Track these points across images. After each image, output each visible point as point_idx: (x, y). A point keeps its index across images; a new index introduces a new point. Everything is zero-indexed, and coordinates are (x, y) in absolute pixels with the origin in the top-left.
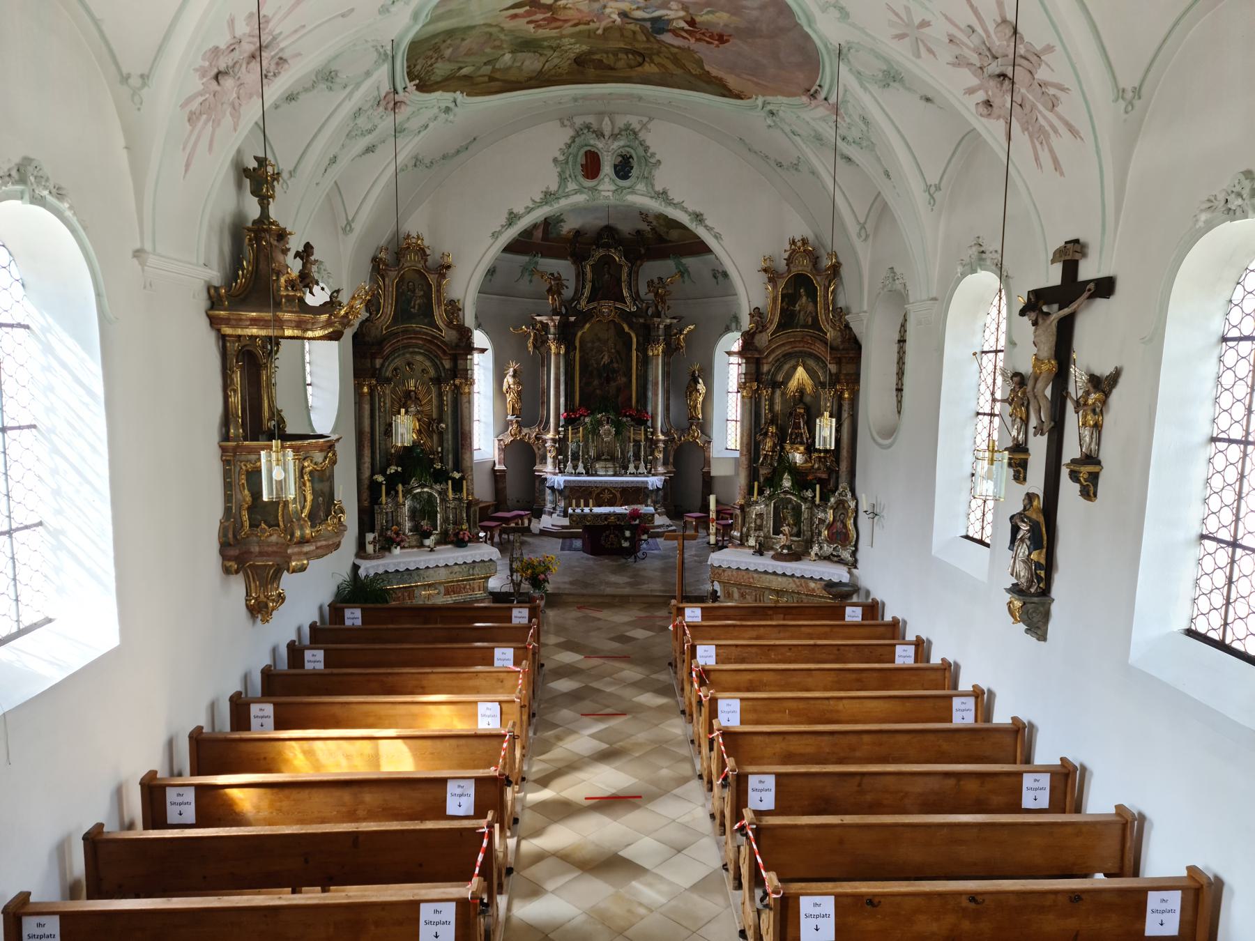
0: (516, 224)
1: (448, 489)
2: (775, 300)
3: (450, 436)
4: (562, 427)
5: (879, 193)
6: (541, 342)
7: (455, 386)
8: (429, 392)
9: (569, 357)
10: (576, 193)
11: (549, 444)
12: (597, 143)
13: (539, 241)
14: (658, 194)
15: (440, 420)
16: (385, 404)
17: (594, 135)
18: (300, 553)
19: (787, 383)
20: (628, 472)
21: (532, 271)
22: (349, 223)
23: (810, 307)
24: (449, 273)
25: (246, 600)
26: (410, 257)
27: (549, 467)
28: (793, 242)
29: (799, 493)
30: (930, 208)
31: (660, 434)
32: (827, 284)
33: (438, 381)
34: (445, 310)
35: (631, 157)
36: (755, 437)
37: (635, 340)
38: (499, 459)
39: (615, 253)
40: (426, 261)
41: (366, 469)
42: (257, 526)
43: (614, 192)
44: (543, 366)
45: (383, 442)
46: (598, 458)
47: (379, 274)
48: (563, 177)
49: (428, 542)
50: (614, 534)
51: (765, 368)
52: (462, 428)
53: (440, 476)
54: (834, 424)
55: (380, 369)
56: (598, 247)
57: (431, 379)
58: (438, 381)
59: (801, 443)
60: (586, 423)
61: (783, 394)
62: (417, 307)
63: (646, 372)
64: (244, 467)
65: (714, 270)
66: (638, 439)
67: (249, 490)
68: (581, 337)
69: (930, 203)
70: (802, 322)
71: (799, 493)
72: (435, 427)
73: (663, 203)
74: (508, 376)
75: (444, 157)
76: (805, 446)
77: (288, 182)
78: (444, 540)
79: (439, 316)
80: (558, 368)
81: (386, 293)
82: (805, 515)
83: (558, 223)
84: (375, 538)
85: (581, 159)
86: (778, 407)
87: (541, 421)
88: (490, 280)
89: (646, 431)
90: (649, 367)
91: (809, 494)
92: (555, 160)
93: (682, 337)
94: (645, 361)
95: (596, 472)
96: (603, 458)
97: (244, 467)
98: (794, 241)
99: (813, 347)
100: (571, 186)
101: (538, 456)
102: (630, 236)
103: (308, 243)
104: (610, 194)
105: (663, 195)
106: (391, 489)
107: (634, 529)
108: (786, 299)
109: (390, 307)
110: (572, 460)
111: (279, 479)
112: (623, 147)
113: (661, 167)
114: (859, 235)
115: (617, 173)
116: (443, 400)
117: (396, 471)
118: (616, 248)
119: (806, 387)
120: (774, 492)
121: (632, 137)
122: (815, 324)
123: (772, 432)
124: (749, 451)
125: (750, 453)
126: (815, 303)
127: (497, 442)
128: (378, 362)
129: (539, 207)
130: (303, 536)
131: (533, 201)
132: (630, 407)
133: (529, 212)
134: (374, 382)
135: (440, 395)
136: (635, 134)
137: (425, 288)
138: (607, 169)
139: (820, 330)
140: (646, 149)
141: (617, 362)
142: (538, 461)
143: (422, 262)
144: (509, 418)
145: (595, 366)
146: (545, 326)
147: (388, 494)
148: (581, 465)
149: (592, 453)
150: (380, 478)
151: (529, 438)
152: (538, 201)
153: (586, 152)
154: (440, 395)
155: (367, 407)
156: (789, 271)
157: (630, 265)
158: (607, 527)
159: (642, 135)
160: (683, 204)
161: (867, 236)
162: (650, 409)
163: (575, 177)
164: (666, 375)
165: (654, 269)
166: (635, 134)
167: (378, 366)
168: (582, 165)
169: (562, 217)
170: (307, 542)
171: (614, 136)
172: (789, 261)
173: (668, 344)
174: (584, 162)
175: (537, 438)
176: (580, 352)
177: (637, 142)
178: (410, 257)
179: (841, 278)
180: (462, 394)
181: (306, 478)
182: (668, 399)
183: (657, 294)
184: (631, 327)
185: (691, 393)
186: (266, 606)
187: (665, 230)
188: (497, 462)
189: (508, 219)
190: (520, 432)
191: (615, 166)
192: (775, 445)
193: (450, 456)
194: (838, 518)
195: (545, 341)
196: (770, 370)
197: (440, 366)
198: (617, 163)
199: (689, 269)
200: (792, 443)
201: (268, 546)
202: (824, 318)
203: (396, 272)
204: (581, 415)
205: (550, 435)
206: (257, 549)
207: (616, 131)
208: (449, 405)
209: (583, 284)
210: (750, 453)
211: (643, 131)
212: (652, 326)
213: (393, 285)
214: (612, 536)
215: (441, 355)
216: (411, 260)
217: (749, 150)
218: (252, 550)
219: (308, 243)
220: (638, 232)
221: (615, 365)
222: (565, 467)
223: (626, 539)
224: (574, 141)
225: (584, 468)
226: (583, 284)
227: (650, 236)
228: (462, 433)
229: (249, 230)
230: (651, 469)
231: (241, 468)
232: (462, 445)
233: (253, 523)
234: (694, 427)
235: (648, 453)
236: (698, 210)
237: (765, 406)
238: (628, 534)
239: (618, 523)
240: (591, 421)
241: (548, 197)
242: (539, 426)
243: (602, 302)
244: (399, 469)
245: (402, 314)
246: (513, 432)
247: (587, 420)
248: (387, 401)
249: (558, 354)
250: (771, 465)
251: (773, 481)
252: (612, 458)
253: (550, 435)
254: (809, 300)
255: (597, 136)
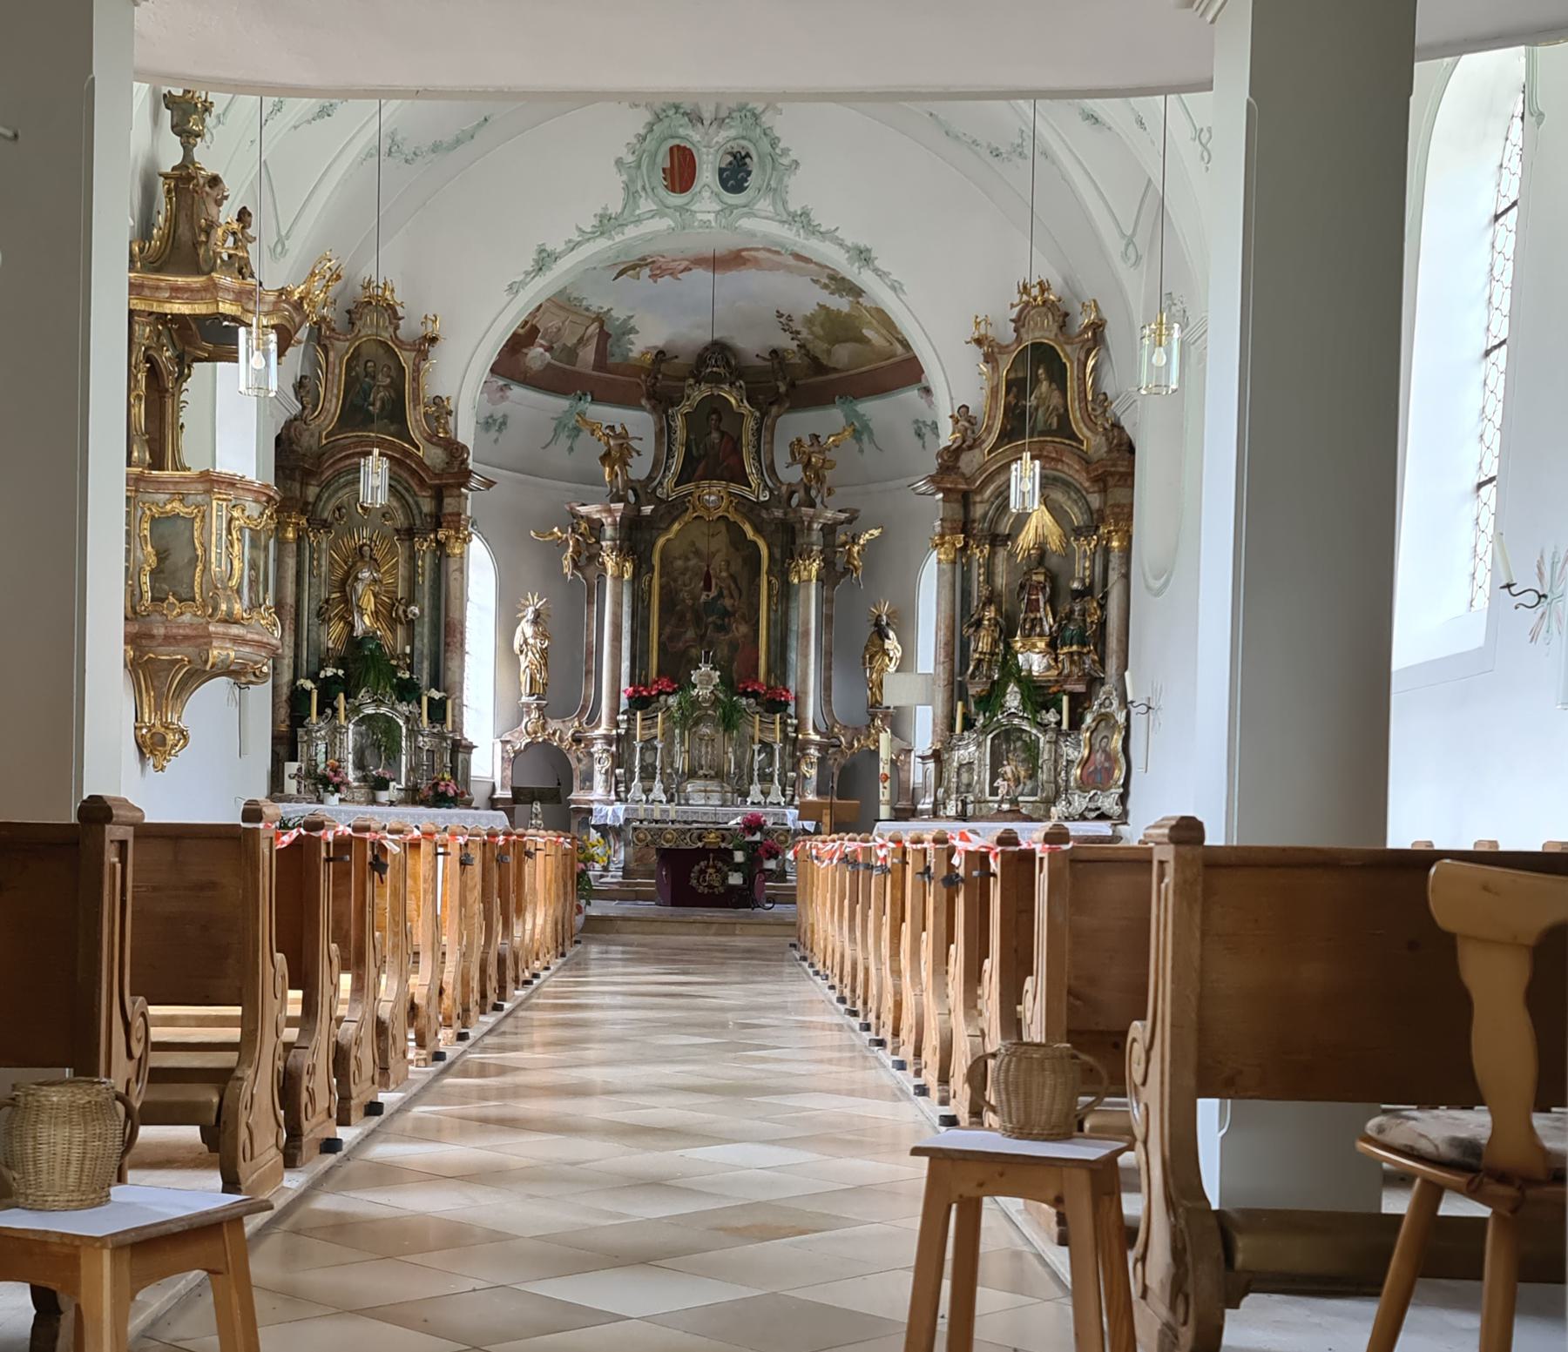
0: (550, 269)
1: (420, 714)
2: (994, 392)
3: (426, 631)
4: (623, 713)
5: (1150, 180)
6: (587, 558)
7: (438, 542)
8: (392, 552)
9: (640, 583)
10: (652, 217)
11: (598, 747)
12: (691, 133)
13: (589, 371)
14: (794, 216)
15: (411, 601)
16: (319, 565)
17: (686, 119)
18: (225, 636)
19: (1017, 536)
20: (749, 800)
21: (575, 428)
22: (281, 241)
23: (1056, 399)
24: (434, 351)
25: (136, 728)
26: (371, 320)
27: (599, 790)
28: (1025, 289)
29: (1034, 717)
30: (1203, 166)
31: (811, 731)
32: (1083, 358)
33: (408, 534)
34: (426, 414)
35: (748, 155)
36: (962, 631)
37: (764, 552)
38: (503, 778)
39: (730, 393)
40: (397, 328)
41: (286, 668)
42: (163, 600)
43: (717, 213)
44: (590, 603)
45: (313, 635)
46: (692, 774)
47: (319, 344)
48: (632, 189)
49: (383, 796)
50: (714, 867)
51: (978, 511)
52: (447, 615)
53: (407, 691)
54: (1037, 470)
55: (315, 504)
56: (698, 382)
57: (397, 531)
58: (408, 534)
59: (1041, 635)
60: (668, 708)
61: (1012, 555)
62: (378, 404)
63: (786, 614)
64: (148, 512)
65: (916, 422)
66: (769, 740)
67: (152, 547)
68: (664, 546)
69: (1203, 158)
70: (1040, 426)
71: (1034, 717)
72: (401, 612)
73: (801, 231)
74: (523, 623)
75: (435, 148)
76: (1047, 639)
77: (214, 131)
78: (413, 796)
79: (415, 419)
80: (618, 604)
81: (329, 376)
82: (1045, 754)
83: (624, 334)
84: (300, 769)
85: (663, 160)
86: (1001, 581)
87: (584, 708)
88: (496, 441)
89: (784, 723)
90: (793, 605)
91: (1051, 717)
92: (619, 162)
93: (856, 549)
94: (785, 594)
95: (687, 800)
96: (701, 773)
97: (148, 512)
98: (1025, 287)
99: (1059, 467)
100: (646, 205)
101: (576, 774)
102: (759, 362)
103: (244, 208)
104: (711, 217)
105: (803, 220)
106: (326, 703)
107: (753, 851)
108: (1014, 389)
109: (334, 400)
110: (642, 779)
111: (258, 367)
112: (735, 139)
113: (798, 172)
114: (1125, 255)
115: (724, 183)
116: (415, 566)
117: (336, 674)
118: (732, 384)
119: (1050, 539)
120: (991, 719)
121: (750, 121)
122: (1064, 428)
123: (989, 620)
124: (950, 656)
125: (952, 660)
126: (1063, 391)
127: (499, 746)
128: (312, 492)
129: (589, 240)
130: (230, 613)
131: (580, 230)
132: (756, 680)
133: (573, 249)
134: (303, 522)
135: (412, 557)
136: (756, 117)
137: (393, 373)
138: (707, 175)
139: (1073, 437)
140: (774, 143)
141: (732, 596)
142: (576, 783)
143: (391, 330)
144: (524, 699)
145: (689, 602)
146: (596, 527)
147: (320, 713)
148: (658, 786)
149: (679, 764)
150: (309, 685)
151: (561, 740)
152: (589, 230)
153: (671, 149)
154: (412, 557)
155: (291, 563)
156: (1019, 340)
157: (758, 414)
158: (703, 853)
159: (766, 120)
160: (837, 234)
161: (1138, 258)
162: (792, 684)
163: (653, 190)
164: (826, 621)
165: (797, 425)
166: (756, 117)
167: (311, 499)
168: (664, 170)
169: (632, 323)
170: (235, 623)
171: (720, 121)
172: (1019, 322)
173: (828, 563)
174: (668, 165)
175: (577, 740)
176: (661, 576)
177: (758, 130)
178: (371, 320)
179: (1108, 350)
180: (448, 556)
181: (235, 536)
182: (829, 667)
183: (807, 465)
184: (758, 530)
185: (872, 657)
186: (163, 742)
187: (825, 346)
188: (498, 785)
189: (537, 262)
190: (544, 729)
191: (721, 171)
192: (995, 643)
193: (426, 664)
194: (1097, 746)
195: (594, 557)
196: (986, 514)
197: (414, 507)
198: (723, 166)
199: (871, 425)
200: (1026, 636)
201: (179, 627)
202: (1078, 415)
203: (347, 344)
204: (660, 693)
205: (602, 730)
206: (162, 631)
207: (723, 113)
208: (427, 573)
209: (670, 449)
210: (952, 660)
211: (768, 114)
212: (798, 526)
213: (341, 363)
214: (710, 871)
215: (416, 488)
216: (370, 326)
217: (947, 133)
218: (155, 632)
219: (244, 208)
220: (774, 352)
221: (728, 602)
222: (628, 790)
223: (737, 868)
224: (651, 130)
225: (665, 792)
226: (670, 449)
227: (798, 361)
228: (447, 625)
229: (166, 176)
230: (793, 796)
231: (144, 513)
232: (447, 644)
233: (156, 595)
234: (878, 722)
235: (788, 766)
236: (863, 242)
237: (978, 575)
238: (739, 857)
239: (723, 845)
240: (680, 703)
241: (606, 224)
242: (580, 716)
243: (705, 483)
244: (341, 672)
245: (354, 414)
246: (529, 729)
247: (672, 701)
248: (323, 563)
249: (618, 578)
250: (989, 677)
251: (990, 700)
252: (719, 775)
253: (602, 730)
254: (1054, 386)
255: (691, 121)
